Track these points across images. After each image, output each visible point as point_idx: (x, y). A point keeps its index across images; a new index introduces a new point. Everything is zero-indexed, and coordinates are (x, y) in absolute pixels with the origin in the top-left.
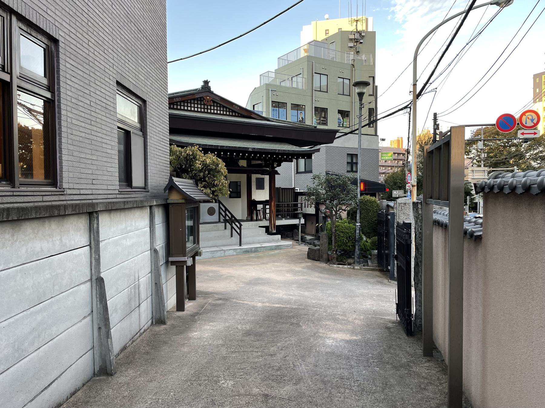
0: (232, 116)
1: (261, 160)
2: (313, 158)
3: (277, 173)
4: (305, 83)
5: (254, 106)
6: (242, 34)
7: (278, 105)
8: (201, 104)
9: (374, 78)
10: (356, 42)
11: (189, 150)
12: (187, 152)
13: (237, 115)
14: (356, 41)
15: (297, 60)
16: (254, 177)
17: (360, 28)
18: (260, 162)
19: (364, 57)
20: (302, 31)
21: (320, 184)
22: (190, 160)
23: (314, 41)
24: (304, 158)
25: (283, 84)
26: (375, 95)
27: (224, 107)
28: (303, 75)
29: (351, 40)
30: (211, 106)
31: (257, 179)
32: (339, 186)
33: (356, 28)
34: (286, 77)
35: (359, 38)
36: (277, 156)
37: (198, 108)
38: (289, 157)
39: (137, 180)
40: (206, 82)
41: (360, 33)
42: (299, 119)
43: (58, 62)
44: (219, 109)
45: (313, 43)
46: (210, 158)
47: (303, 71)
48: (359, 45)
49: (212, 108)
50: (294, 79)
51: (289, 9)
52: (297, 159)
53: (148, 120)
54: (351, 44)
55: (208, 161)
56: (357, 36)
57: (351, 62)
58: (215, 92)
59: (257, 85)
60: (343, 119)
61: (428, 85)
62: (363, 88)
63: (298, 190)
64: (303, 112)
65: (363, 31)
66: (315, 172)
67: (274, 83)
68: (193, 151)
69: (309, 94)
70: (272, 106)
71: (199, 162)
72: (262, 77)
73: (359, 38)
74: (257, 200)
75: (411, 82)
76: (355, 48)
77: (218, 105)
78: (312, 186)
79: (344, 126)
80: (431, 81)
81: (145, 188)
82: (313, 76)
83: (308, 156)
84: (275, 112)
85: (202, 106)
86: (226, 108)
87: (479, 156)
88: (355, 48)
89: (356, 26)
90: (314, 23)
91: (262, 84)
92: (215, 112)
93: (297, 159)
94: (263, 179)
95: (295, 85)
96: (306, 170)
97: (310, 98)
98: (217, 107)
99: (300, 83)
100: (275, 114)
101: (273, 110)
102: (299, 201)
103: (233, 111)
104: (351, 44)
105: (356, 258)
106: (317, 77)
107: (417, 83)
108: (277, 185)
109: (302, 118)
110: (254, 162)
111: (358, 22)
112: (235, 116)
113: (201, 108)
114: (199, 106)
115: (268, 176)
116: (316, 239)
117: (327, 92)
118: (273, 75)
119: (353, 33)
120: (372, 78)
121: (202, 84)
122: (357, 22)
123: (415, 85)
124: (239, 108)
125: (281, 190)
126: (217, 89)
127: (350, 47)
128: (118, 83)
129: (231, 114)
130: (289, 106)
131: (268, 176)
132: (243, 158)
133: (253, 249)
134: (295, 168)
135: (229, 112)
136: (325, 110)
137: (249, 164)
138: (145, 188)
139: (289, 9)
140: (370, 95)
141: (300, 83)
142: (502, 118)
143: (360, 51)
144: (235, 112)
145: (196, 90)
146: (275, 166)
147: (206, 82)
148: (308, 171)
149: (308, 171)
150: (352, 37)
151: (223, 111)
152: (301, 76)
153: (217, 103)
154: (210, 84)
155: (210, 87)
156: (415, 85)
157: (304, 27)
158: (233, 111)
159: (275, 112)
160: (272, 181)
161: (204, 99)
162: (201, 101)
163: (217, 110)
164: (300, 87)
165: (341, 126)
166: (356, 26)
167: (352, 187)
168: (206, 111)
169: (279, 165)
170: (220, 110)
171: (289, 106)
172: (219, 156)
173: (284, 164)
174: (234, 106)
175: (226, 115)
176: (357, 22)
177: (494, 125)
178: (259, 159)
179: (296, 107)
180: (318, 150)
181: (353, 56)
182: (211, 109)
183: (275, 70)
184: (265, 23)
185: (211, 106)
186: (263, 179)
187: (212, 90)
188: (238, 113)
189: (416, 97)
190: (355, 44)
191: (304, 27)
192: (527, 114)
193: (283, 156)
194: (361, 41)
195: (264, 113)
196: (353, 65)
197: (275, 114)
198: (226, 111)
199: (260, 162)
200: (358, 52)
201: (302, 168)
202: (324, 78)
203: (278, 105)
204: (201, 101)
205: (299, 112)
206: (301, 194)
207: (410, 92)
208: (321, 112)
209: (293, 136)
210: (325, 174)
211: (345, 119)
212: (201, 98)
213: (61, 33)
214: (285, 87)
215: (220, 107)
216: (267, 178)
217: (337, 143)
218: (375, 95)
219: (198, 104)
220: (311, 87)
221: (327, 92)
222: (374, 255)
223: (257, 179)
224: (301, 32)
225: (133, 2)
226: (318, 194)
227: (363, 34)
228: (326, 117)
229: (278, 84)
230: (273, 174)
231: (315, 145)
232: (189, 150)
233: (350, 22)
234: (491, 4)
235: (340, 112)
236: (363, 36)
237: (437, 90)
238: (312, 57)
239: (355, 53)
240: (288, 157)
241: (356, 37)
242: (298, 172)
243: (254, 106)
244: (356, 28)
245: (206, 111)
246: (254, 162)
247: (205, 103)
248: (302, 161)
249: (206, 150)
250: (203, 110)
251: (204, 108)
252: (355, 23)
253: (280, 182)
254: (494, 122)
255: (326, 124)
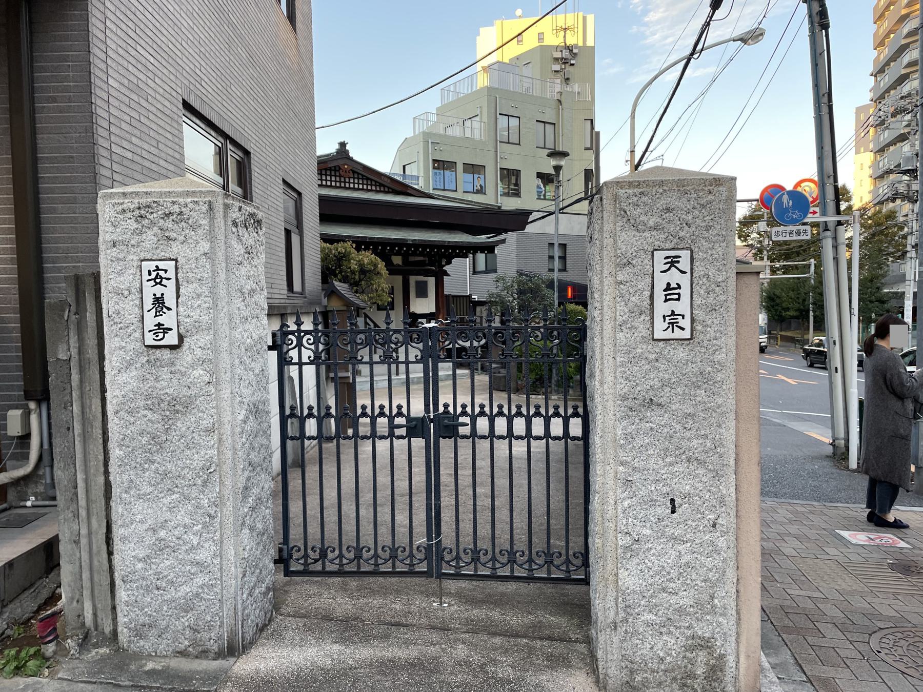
0: (380, 192)
1: (424, 256)
2: (496, 252)
3: (447, 274)
4: (485, 130)
5: (404, 167)
6: (402, 99)
7: (440, 165)
8: (335, 176)
9: (592, 121)
10: (565, 63)
11: (341, 247)
12: (339, 249)
13: (386, 190)
14: (565, 61)
15: (472, 93)
16: (413, 279)
17: (571, 41)
18: (421, 258)
19: (576, 88)
20: (479, 35)
21: (506, 288)
22: (342, 258)
23: (498, 62)
24: (484, 252)
25: (450, 132)
26: (594, 149)
27: (368, 179)
28: (481, 118)
29: (556, 59)
30: (349, 178)
31: (417, 283)
32: (531, 291)
33: (565, 40)
34: (455, 121)
35: (569, 56)
36: (447, 250)
37: (331, 181)
38: (463, 251)
39: (297, 287)
40: (343, 145)
41: (569, 48)
42: (475, 188)
43: (250, 173)
44: (361, 182)
45: (496, 67)
46: (367, 257)
47: (481, 112)
48: (568, 68)
49: (352, 181)
50: (468, 123)
51: (462, 71)
52: (474, 254)
53: (304, 215)
54: (557, 67)
55: (366, 261)
56: (566, 54)
57: (557, 97)
58: (355, 158)
59: (410, 134)
60: (545, 187)
61: (648, 153)
62: (560, 160)
63: (476, 297)
64: (482, 177)
65: (576, 46)
66: (500, 272)
67: (436, 131)
68: (345, 249)
69: (491, 147)
70: (434, 168)
71: (355, 262)
72: (417, 121)
73: (569, 56)
74: (418, 312)
75: (628, 147)
76: (562, 74)
77: (360, 177)
78: (495, 291)
79: (547, 197)
80: (651, 148)
81: (302, 293)
82: (496, 119)
83: (489, 249)
84: (438, 177)
85: (338, 179)
86: (372, 180)
87: (760, 242)
88: (562, 74)
89: (565, 37)
90: (498, 23)
91: (417, 133)
92: (356, 186)
93: (474, 254)
94: (426, 282)
95: (468, 134)
96: (488, 269)
97: (492, 154)
98: (358, 179)
99: (476, 130)
100: (438, 180)
101: (436, 174)
102: (478, 314)
103: (381, 185)
104: (557, 67)
105: (553, 386)
106: (502, 121)
107: (636, 149)
108: (446, 292)
109: (481, 186)
110: (412, 259)
111: (568, 32)
112: (384, 192)
113: (336, 181)
114: (333, 178)
115: (434, 278)
116: (502, 368)
117: (519, 144)
118: (435, 118)
119: (559, 49)
120: (589, 122)
121: (337, 147)
122: (565, 32)
123: (632, 152)
124: (389, 181)
125: (451, 299)
126: (358, 154)
127: (555, 71)
128: (284, 181)
129: (378, 189)
130: (460, 167)
131: (434, 278)
132: (398, 254)
133: (415, 380)
134: (472, 266)
135: (376, 186)
136: (517, 173)
137: (405, 261)
138: (302, 293)
139: (462, 71)
140: (586, 149)
141: (476, 130)
142: (769, 190)
143: (570, 77)
144: (384, 186)
145: (328, 155)
146: (444, 263)
147: (343, 145)
148: (491, 269)
149: (491, 269)
150: (558, 55)
151: (367, 185)
152: (477, 119)
153: (358, 174)
154: (348, 148)
155: (348, 151)
156: (632, 152)
157: (482, 30)
158: (381, 185)
159: (438, 177)
160: (439, 286)
161: (340, 169)
162: (335, 171)
163: (358, 184)
164: (477, 136)
165: (542, 197)
166: (565, 37)
167: (547, 292)
168: (343, 185)
169: (449, 263)
170: (363, 184)
171: (460, 167)
172: (375, 252)
173: (455, 261)
174: (383, 177)
175: (371, 190)
176: (565, 32)
177: (757, 200)
178: (421, 254)
179: (473, 169)
180: (503, 241)
181: (559, 86)
182: (349, 183)
183: (438, 109)
184: (432, 87)
185: (349, 178)
186: (426, 282)
187: (351, 155)
188: (389, 188)
189: (634, 169)
190: (563, 67)
191: (482, 30)
192: (802, 185)
193: (454, 250)
194: (572, 62)
195: (420, 178)
196: (560, 101)
197: (438, 180)
198: (371, 185)
199: (421, 258)
200: (568, 79)
201: (481, 266)
202: (514, 122)
203: (440, 165)
204: (335, 171)
205: (476, 176)
206: (481, 303)
207: (627, 161)
208: (511, 178)
209: (468, 222)
210: (515, 274)
211: (547, 188)
212: (335, 167)
213: (252, 145)
214: (454, 138)
215: (363, 179)
216: (431, 281)
217: (529, 228)
218: (594, 149)
219: (331, 176)
220: (493, 138)
221: (519, 144)
222: (576, 381)
223: (417, 283)
224: (478, 37)
225: (207, 3)
226: (502, 302)
227: (575, 51)
228: (517, 184)
229: (442, 132)
230: (440, 276)
231: (500, 234)
232: (341, 247)
233: (555, 31)
234: (734, 41)
235: (540, 175)
236: (575, 54)
237: (664, 157)
238: (494, 89)
239: (563, 80)
240: (461, 251)
241: (564, 56)
242: (475, 272)
243: (404, 167)
244: (565, 40)
245: (343, 185)
246: (412, 259)
247: (342, 174)
248: (481, 257)
249: (361, 244)
250: (338, 184)
251: (340, 182)
252: (562, 33)
253: (451, 287)
254: (757, 196)
255: (517, 194)
